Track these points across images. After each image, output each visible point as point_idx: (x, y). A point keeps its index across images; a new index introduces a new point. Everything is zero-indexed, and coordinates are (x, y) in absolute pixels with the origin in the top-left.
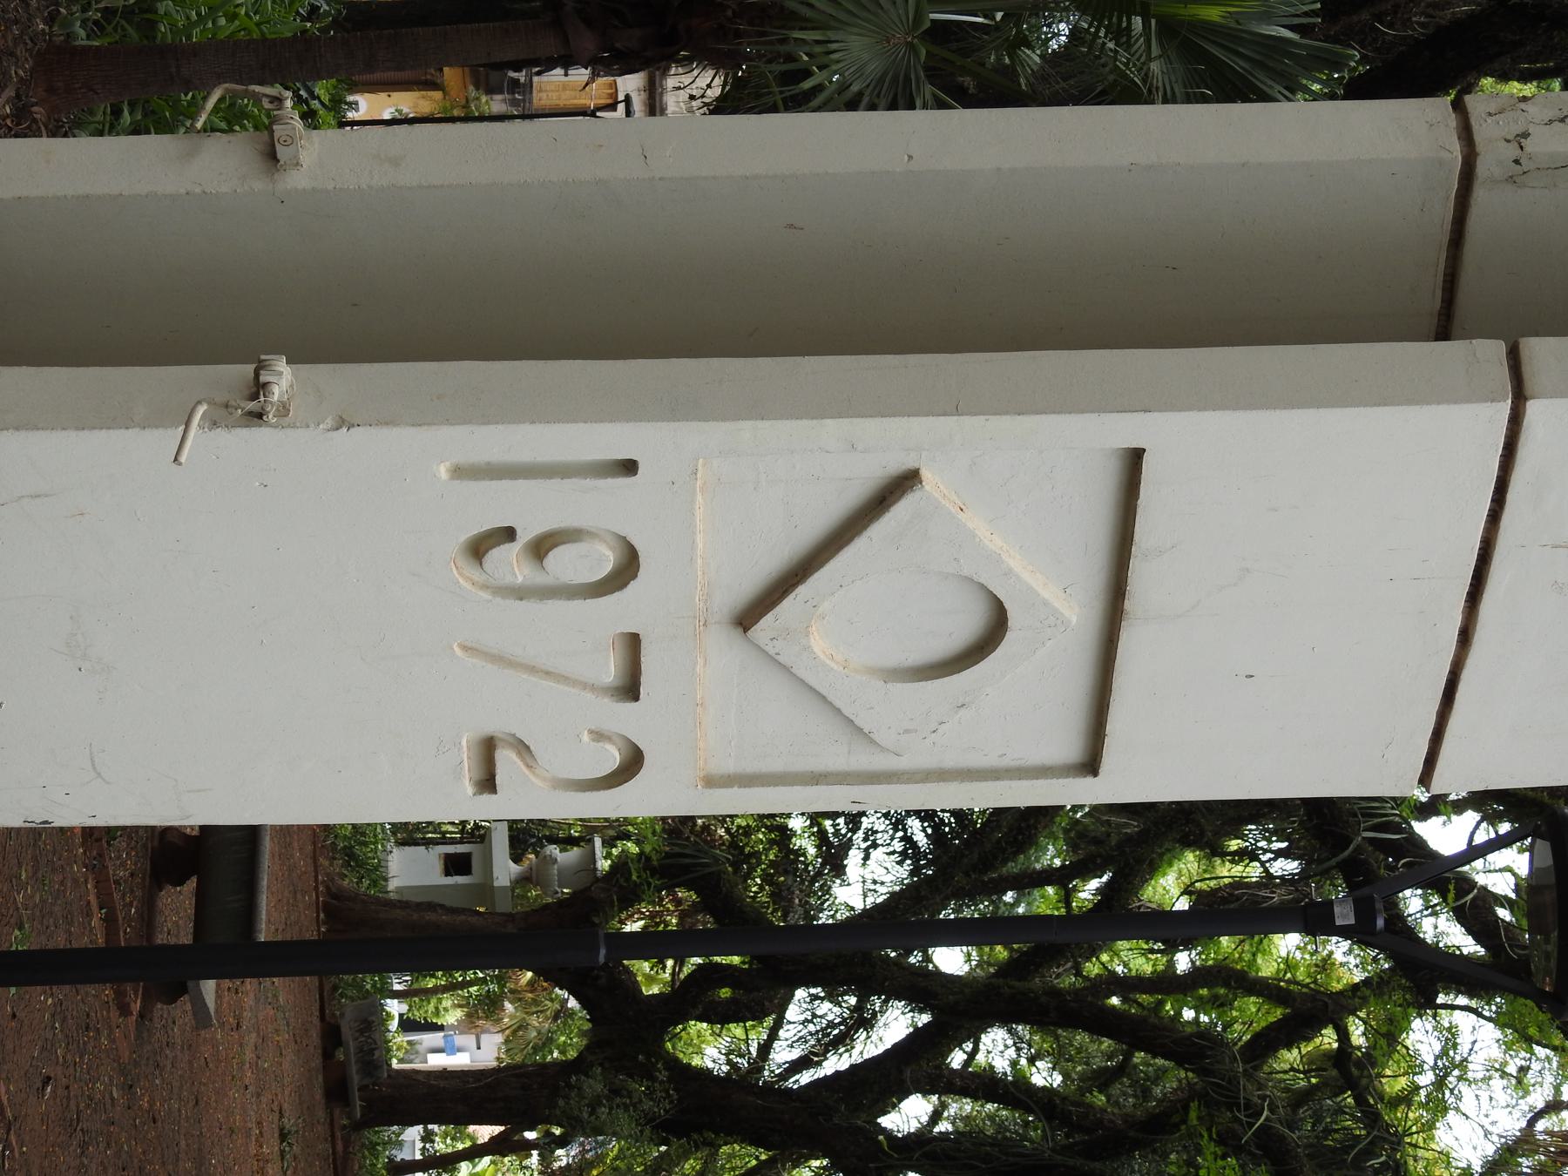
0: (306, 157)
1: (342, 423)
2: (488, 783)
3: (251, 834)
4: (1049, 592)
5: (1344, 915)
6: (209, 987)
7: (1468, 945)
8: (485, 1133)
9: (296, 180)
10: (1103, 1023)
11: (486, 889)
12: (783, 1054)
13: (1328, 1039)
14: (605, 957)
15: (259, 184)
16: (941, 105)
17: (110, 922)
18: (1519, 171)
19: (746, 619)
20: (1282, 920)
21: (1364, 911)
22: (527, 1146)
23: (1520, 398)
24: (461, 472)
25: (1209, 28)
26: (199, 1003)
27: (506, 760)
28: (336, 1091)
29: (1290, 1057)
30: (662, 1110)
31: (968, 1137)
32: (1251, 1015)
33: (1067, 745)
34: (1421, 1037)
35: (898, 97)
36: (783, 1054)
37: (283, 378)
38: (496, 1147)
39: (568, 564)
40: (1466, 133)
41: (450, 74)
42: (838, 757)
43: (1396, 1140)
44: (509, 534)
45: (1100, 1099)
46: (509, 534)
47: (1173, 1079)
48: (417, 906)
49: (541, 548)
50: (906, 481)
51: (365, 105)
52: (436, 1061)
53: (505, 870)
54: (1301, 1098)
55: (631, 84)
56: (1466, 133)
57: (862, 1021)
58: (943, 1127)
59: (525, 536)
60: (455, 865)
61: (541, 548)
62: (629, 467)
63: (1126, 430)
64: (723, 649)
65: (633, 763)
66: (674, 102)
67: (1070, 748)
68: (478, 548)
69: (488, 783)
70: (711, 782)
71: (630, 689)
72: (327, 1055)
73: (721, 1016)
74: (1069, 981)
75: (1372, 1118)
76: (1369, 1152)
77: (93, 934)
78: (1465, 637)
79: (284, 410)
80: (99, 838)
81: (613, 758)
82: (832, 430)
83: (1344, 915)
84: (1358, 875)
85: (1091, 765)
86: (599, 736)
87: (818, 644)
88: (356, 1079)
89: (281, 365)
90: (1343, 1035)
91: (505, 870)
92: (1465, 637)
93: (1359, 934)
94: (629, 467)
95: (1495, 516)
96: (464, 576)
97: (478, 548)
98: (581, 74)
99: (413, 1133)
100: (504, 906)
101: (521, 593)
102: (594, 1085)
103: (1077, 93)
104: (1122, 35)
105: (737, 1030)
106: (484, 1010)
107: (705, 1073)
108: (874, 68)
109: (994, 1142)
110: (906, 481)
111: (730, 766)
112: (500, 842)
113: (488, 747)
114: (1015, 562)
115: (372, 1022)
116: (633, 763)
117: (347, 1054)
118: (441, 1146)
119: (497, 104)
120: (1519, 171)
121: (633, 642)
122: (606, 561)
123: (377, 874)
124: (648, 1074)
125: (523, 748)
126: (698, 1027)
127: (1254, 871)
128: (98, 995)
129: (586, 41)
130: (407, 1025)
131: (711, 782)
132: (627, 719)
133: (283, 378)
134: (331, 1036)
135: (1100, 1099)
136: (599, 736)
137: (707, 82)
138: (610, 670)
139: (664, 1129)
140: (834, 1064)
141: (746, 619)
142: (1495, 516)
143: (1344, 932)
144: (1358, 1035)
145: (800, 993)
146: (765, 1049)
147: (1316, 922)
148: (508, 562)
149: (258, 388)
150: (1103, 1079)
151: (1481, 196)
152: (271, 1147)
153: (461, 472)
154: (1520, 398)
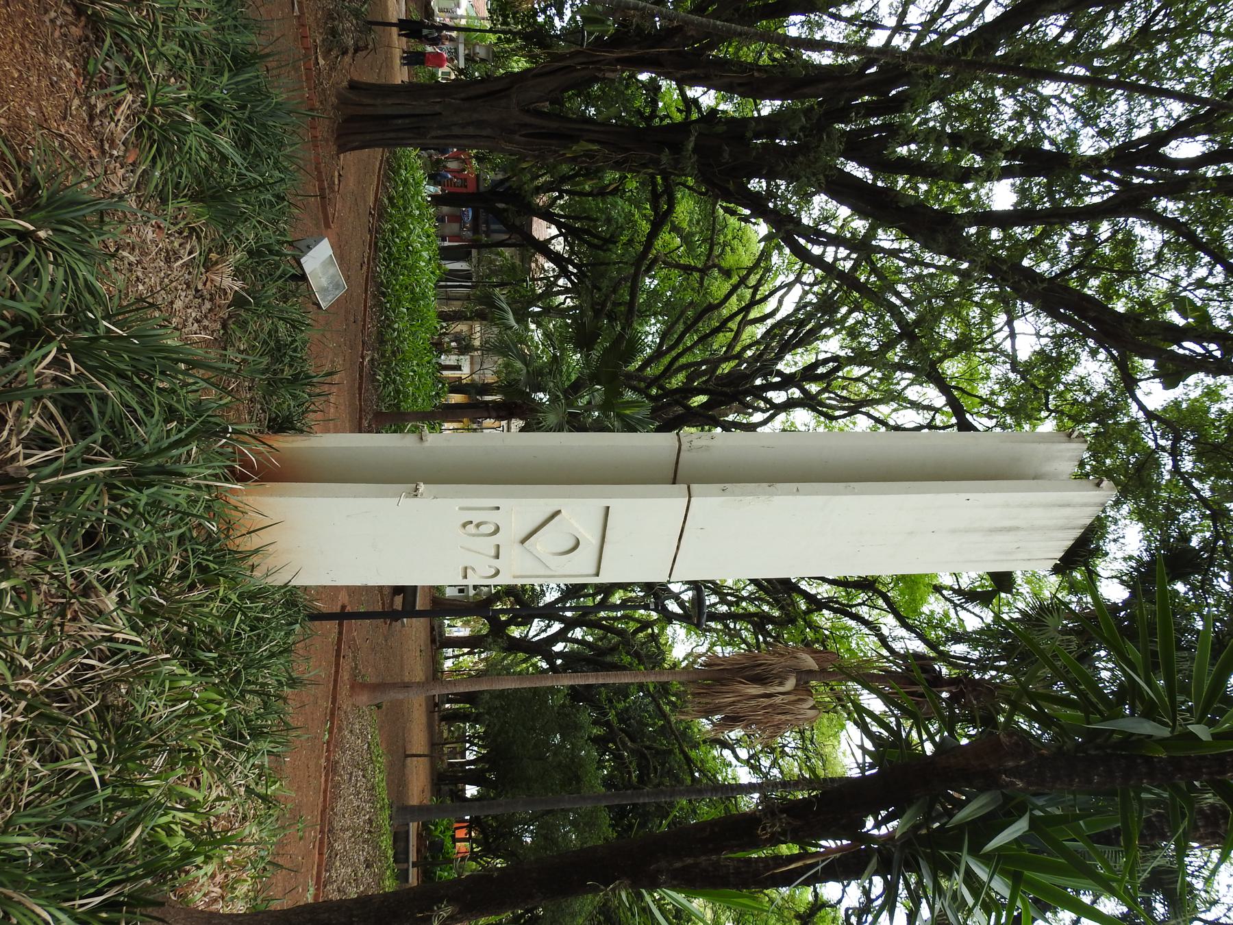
0: (429, 439)
1: (435, 497)
2: (465, 577)
3: (416, 587)
4: (589, 537)
5: (652, 606)
6: (405, 620)
7: (680, 611)
8: (466, 650)
9: (426, 444)
10: (601, 627)
11: (467, 597)
12: (531, 634)
13: (650, 631)
14: (1109, 46)
15: (419, 445)
16: (571, 431)
17: (383, 604)
18: (690, 449)
19: (523, 542)
20: (640, 607)
21: (656, 605)
22: (475, 653)
23: (690, 497)
24: (461, 509)
25: (628, 416)
26: (403, 622)
27: (469, 571)
28: (433, 641)
29: (641, 635)
30: (505, 645)
31: (572, 651)
32: (632, 626)
33: (593, 570)
34: (669, 630)
35: (560, 429)
36: (531, 634)
37: (422, 487)
38: (469, 653)
39: (485, 529)
40: (679, 440)
41: (465, 420)
42: (542, 572)
43: (663, 653)
44: (471, 522)
45: (600, 643)
46: (471, 522)
47: (616, 639)
48: (452, 601)
49: (478, 526)
50: (558, 512)
51: (446, 425)
52: (456, 634)
53: (472, 592)
54: (643, 644)
55: (504, 423)
56: (679, 440)
57: (549, 626)
58: (566, 650)
59: (474, 523)
60: (461, 591)
61: (478, 526)
62: (498, 508)
63: (606, 502)
64: (518, 548)
65: (497, 573)
66: (513, 426)
67: (593, 571)
68: (464, 525)
69: (465, 577)
70: (514, 577)
71: (497, 557)
72: (431, 633)
73: (518, 625)
74: (593, 618)
75: (659, 648)
76: (658, 655)
77: (379, 608)
78: (678, 548)
79: (422, 494)
80: (381, 588)
81: (493, 571)
82: (542, 501)
83: (652, 606)
84: (656, 596)
85: (597, 574)
86: (490, 567)
87: (539, 548)
88: (438, 638)
89: (422, 484)
90: (653, 630)
91: (472, 592)
92: (678, 548)
93: (655, 610)
94: (498, 508)
95: (684, 522)
96: (461, 531)
97: (464, 525)
98: (492, 421)
99: (451, 650)
100: (471, 600)
101: (474, 535)
102: (490, 640)
103: (69, 355)
104: (608, 417)
105: (522, 628)
106: (466, 624)
107: (515, 638)
108: (556, 421)
109: (578, 653)
110: (558, 512)
111: (519, 574)
112: (471, 589)
113: (466, 569)
114: (581, 530)
115: (441, 626)
116: (497, 573)
117: (436, 632)
118: (456, 653)
119: (475, 426)
120: (690, 449)
121: (498, 546)
122: (492, 529)
123: (444, 594)
124: (502, 638)
125: (473, 569)
126: (513, 627)
127: (634, 595)
128: (380, 622)
129: (494, 414)
130: (449, 626)
131: (514, 577)
132: (496, 563)
133: (422, 487)
134: (432, 629)
135: (600, 643)
136: (490, 567)
137: (521, 423)
138: (493, 553)
139: (506, 650)
140: (543, 635)
141: (523, 542)
142: (684, 522)
143: (652, 610)
144: (656, 631)
145: (536, 620)
146: (528, 632)
147: (646, 607)
148: (471, 528)
149: (416, 490)
150: (601, 639)
151: (682, 454)
152: (418, 653)
153: (461, 509)
154: (690, 497)
